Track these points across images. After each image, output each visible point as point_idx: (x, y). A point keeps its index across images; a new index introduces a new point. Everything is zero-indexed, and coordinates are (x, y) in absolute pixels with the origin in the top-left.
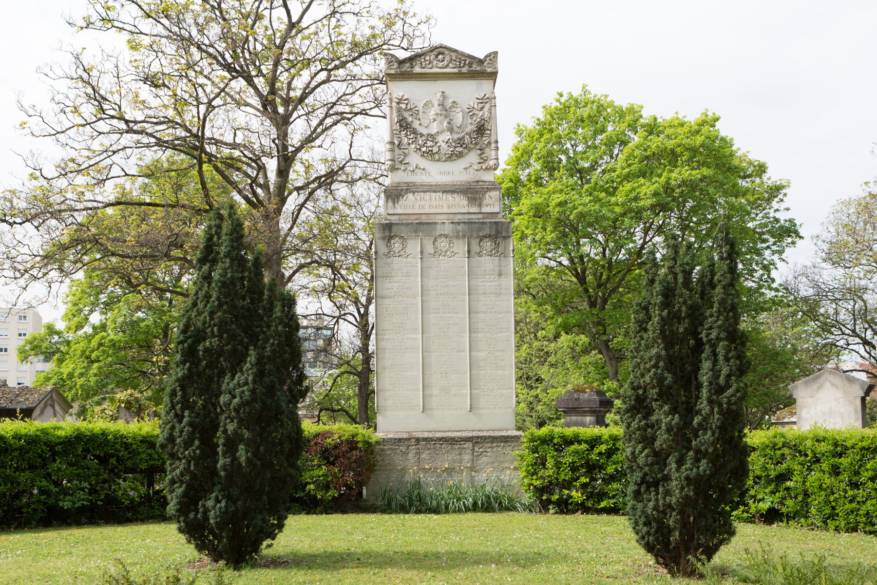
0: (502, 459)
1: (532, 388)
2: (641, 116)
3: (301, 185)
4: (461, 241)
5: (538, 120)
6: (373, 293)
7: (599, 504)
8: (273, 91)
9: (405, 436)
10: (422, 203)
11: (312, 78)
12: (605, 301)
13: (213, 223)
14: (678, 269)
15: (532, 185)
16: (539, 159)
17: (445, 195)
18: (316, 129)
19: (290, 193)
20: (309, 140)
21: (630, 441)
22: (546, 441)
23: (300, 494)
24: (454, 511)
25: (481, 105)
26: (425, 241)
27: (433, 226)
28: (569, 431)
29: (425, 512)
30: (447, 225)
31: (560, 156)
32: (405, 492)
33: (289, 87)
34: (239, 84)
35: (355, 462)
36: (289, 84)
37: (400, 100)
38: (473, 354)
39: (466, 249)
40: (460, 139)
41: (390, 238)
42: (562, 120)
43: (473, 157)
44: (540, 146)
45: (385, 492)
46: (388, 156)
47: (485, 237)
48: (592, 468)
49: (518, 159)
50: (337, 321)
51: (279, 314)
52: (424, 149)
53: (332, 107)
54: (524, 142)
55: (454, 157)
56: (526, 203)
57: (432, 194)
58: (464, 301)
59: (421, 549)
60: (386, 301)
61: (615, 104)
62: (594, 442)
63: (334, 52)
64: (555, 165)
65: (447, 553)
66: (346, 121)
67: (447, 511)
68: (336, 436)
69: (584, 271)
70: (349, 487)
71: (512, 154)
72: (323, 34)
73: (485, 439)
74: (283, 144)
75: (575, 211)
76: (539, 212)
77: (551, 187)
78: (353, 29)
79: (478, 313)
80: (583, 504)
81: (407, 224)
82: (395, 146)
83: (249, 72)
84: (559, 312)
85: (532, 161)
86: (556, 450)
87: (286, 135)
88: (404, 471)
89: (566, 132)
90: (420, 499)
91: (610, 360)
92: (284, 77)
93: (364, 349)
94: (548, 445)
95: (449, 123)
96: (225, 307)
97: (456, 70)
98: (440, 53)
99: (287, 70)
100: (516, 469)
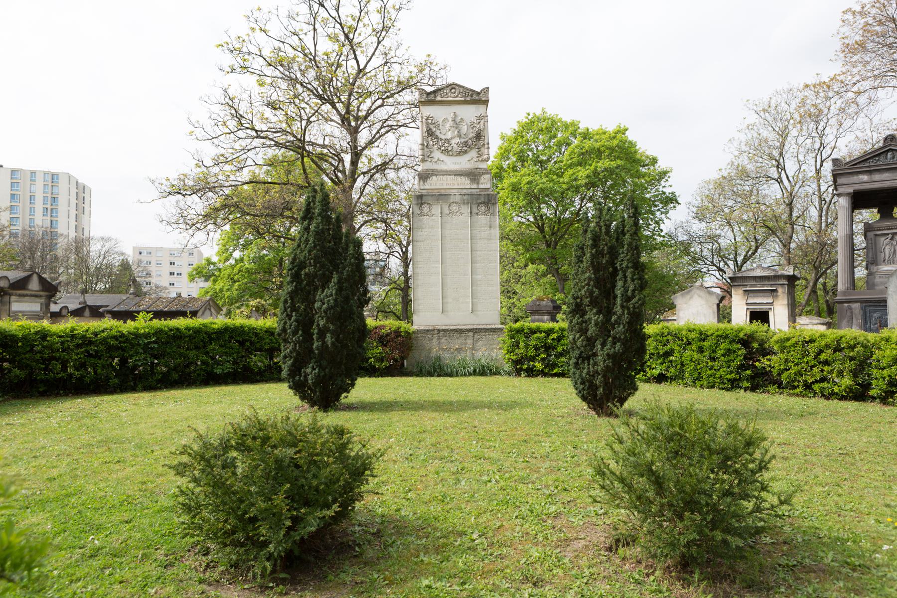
1: (510, 298)
4: (466, 206)
6: (411, 239)
8: (348, 112)
12: (556, 244)
14: (602, 224)
15: (510, 171)
19: (359, 176)
20: (371, 143)
22: (519, 331)
23: (365, 365)
24: (462, 375)
28: (534, 325)
34: (327, 107)
36: (358, 107)
41: (422, 204)
43: (473, 153)
46: (420, 152)
48: (548, 348)
49: (502, 155)
56: (506, 182)
59: (441, 399)
60: (419, 244)
62: (549, 332)
63: (386, 87)
65: (457, 401)
67: (457, 375)
69: (543, 225)
70: (396, 360)
72: (380, 76)
76: (515, 188)
80: (542, 371)
82: (425, 146)
84: (527, 250)
87: (356, 139)
88: (430, 350)
92: (355, 103)
93: (405, 273)
100: (500, 349)
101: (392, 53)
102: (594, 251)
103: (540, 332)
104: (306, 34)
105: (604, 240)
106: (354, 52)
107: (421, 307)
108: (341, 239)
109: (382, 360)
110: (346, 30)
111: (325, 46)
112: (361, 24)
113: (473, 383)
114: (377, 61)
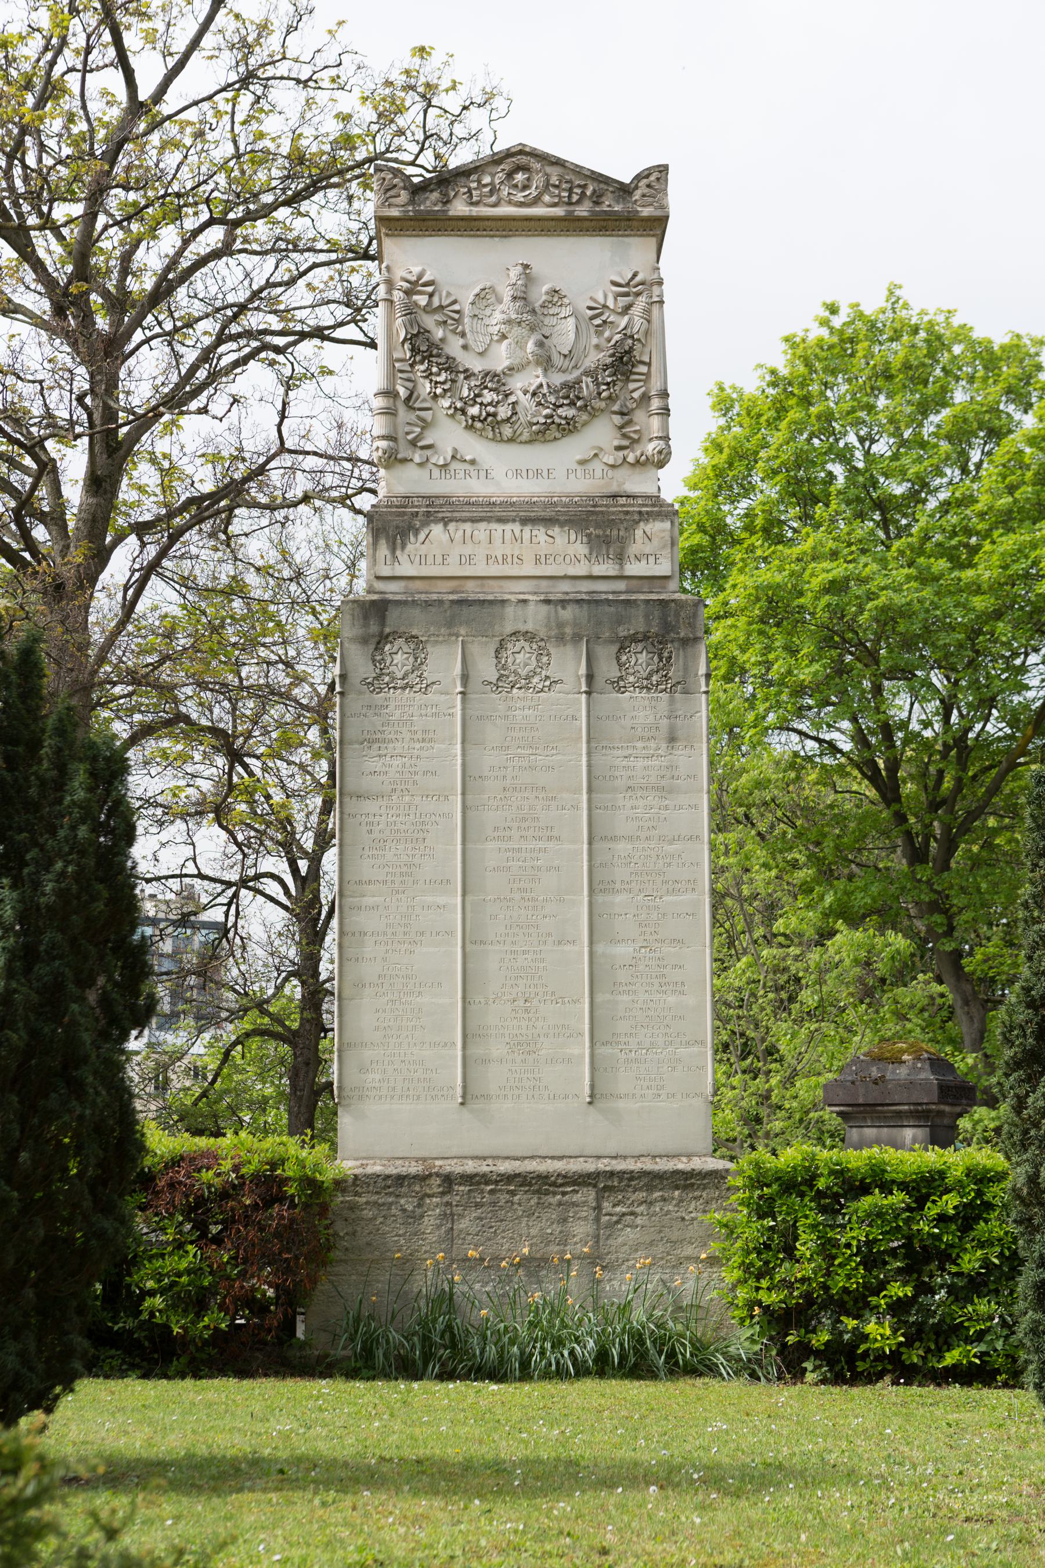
0: (675, 1235)
1: (755, 1074)
3: (147, 517)
4: (569, 650)
5: (773, 372)
6: (333, 822)
7: (941, 1358)
8: (83, 271)
9: (414, 1169)
10: (468, 550)
11: (186, 243)
12: (950, 846)
15: (757, 540)
16: (775, 472)
17: (527, 529)
18: (194, 368)
19: (119, 539)
20: (176, 400)
21: (1025, 1148)
22: (796, 1183)
23: (124, 1323)
24: (546, 1375)
25: (623, 301)
26: (474, 649)
27: (497, 609)
28: (856, 1159)
29: (465, 1377)
30: (531, 607)
31: (830, 467)
32: (411, 1322)
33: (125, 270)
35: (277, 1235)
36: (127, 258)
37: (415, 283)
38: (600, 948)
39: (583, 670)
40: (568, 386)
41: (383, 639)
42: (834, 372)
43: (602, 433)
44: (776, 438)
45: (357, 1320)
46: (378, 426)
47: (634, 639)
48: (921, 1259)
49: (719, 473)
50: (236, 895)
51: (81, 794)
52: (474, 411)
53: (235, 316)
54: (736, 430)
55: (554, 432)
56: (741, 585)
57: (494, 526)
58: (576, 807)
59: (454, 1453)
60: (369, 806)
61: (976, 335)
62: (925, 1187)
63: (244, 179)
64: (817, 490)
65: (525, 1462)
66: (272, 355)
67: (525, 1374)
68: (227, 1165)
69: (893, 766)
70: (259, 1307)
71: (705, 460)
72: (220, 133)
73: (629, 1178)
74: (106, 407)
75: (870, 605)
76: (776, 610)
77: (807, 546)
78: (294, 122)
79: (614, 839)
80: (895, 1356)
81: (428, 604)
82: (396, 400)
83: (20, 215)
84: (827, 874)
85: (756, 479)
86: (823, 1210)
88: (408, 1265)
89: (846, 406)
90: (454, 1340)
91: (966, 1003)
92: (112, 241)
93: (307, 969)
94: (802, 1195)
95: (540, 344)
97: (559, 211)
98: (519, 168)
99: (117, 223)
100: (713, 1261)
101: (273, 43)
103: (886, 1188)
107: (373, 1078)
108: (35, 745)
109: (199, 1303)
113: (596, 1401)
114: (205, 74)
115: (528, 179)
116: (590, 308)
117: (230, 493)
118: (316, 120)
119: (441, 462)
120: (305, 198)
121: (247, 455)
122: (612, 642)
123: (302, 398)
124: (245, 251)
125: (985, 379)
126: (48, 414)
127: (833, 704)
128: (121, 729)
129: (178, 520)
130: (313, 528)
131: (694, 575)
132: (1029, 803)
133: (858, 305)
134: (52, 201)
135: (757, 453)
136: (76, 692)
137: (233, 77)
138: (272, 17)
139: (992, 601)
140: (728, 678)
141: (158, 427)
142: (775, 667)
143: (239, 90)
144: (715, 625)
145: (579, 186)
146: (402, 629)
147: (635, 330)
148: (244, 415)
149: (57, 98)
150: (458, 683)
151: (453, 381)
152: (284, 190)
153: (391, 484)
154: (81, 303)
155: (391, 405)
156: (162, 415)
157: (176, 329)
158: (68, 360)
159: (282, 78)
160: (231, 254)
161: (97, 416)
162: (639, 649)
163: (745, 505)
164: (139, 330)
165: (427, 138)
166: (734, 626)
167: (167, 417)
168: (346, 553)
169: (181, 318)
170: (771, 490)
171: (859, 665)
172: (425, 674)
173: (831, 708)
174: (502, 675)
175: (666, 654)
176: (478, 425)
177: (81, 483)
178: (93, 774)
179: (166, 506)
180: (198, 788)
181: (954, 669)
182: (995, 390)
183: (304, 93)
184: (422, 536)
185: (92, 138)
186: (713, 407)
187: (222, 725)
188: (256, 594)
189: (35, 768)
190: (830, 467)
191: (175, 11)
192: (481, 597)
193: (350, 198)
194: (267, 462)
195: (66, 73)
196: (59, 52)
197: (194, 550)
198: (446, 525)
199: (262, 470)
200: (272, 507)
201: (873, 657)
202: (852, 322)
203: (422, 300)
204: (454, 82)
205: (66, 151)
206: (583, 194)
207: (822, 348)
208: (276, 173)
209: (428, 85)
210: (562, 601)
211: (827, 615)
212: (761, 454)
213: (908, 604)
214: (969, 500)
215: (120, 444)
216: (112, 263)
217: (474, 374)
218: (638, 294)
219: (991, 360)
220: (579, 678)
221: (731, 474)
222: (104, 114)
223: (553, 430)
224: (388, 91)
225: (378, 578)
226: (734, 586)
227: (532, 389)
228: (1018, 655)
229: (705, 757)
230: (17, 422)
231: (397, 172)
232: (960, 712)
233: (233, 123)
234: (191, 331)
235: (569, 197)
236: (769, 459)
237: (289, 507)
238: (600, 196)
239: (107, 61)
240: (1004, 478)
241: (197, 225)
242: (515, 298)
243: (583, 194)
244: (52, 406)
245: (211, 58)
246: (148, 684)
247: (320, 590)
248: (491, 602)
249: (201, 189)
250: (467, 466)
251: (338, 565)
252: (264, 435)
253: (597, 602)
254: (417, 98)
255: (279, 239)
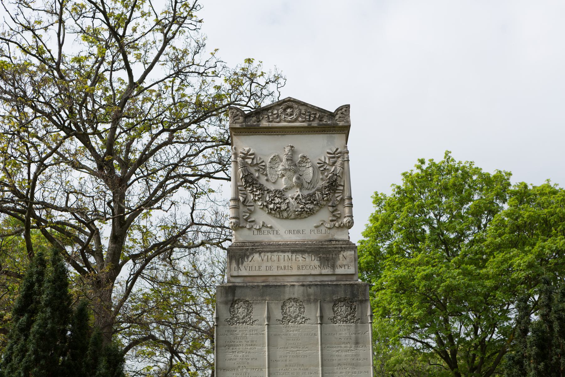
2: (509, 184)
3: (137, 252)
5: (399, 188)
10: (269, 264)
13: (35, 270)
14: (553, 317)
18: (156, 191)
19: (125, 262)
20: (149, 203)
25: (332, 160)
26: (273, 306)
30: (296, 288)
31: (423, 227)
33: (128, 151)
34: (75, 144)
36: (129, 146)
39: (318, 314)
40: (310, 195)
41: (234, 302)
42: (424, 188)
43: (324, 215)
46: (230, 212)
47: (340, 301)
49: (377, 229)
52: (271, 206)
53: (173, 169)
55: (304, 214)
56: (389, 275)
57: (280, 254)
58: (317, 373)
61: (482, 172)
63: (177, 113)
64: (418, 236)
66: (188, 184)
69: (454, 353)
72: (167, 95)
74: (120, 207)
75: (442, 285)
76: (403, 287)
78: (197, 89)
81: (253, 287)
82: (239, 203)
83: (85, 129)
85: (392, 232)
87: (123, 196)
89: (430, 201)
92: (122, 139)
95: (298, 178)
96: (42, 362)
97: (305, 124)
98: (288, 107)
99: (125, 131)
101: (189, 58)
102: (541, 366)
104: (46, 28)
105: (558, 346)
106: (125, 59)
110: (112, 21)
111: (75, 47)
112: (137, 13)
114: (161, 71)
115: (292, 111)
116: (319, 163)
117: (171, 242)
118: (206, 89)
119: (258, 228)
120: (202, 120)
121: (178, 226)
122: (331, 302)
123: (201, 202)
124: (177, 142)
125: (487, 190)
126: (96, 210)
127: (427, 327)
128: (125, 342)
129: (150, 253)
130: (207, 256)
131: (367, 273)
132: (506, 368)
133: (433, 160)
134: (97, 123)
135: (392, 221)
136: (106, 326)
137: (172, 72)
138: (188, 48)
139: (494, 282)
140: (383, 316)
141: (141, 215)
142: (403, 311)
143: (175, 77)
144: (377, 293)
145: (313, 114)
146: (242, 298)
147: (338, 172)
148: (177, 209)
149: (101, 82)
150: (266, 320)
151: (262, 194)
152: (193, 117)
153: (235, 238)
154: (109, 164)
155: (237, 204)
156: (143, 210)
157: (148, 175)
158: (103, 187)
159: (192, 72)
160: (172, 143)
161: (115, 211)
162: (342, 305)
163: (388, 243)
164: (134, 175)
165: (251, 95)
166: (385, 294)
167: (145, 211)
168: (221, 266)
169: (151, 170)
170: (398, 237)
171: (439, 310)
172: (252, 317)
173: (427, 328)
174: (284, 317)
175: (353, 307)
176: (273, 212)
177: (109, 238)
178: (109, 362)
179: (144, 247)
180: (159, 367)
181: (478, 311)
182: (492, 195)
183: (201, 78)
184: (250, 259)
185: (115, 97)
186: (374, 202)
187: (169, 340)
188: (183, 284)
189: (84, 359)
190: (423, 227)
191: (149, 46)
192: (275, 284)
193: (220, 120)
194: (187, 229)
195: (104, 71)
196: (101, 63)
197: (157, 266)
198: (260, 254)
199: (184, 232)
200: (189, 247)
201: (444, 306)
202: (430, 167)
203: (249, 161)
204: (262, 72)
205: (103, 103)
206: (315, 117)
207: (418, 177)
208: (190, 110)
209: (252, 74)
210: (309, 285)
211: (424, 289)
212: (394, 222)
213: (458, 285)
214: (482, 240)
215: (125, 222)
216: (123, 148)
217: (271, 191)
218: (338, 157)
219: (489, 182)
220: (317, 317)
221: (382, 230)
222: (120, 87)
223: (304, 214)
224: (235, 77)
225: (232, 276)
226: (385, 276)
227: (295, 197)
228: (505, 305)
229: (371, 350)
230: (82, 214)
231: (238, 110)
232: (481, 329)
233: (172, 90)
234: (155, 175)
235: (309, 118)
236: (398, 224)
237: (196, 247)
238: (322, 118)
239: (121, 66)
240: (497, 231)
241: (158, 132)
242: (287, 160)
243: (315, 117)
244: (97, 207)
245: (163, 64)
246: (136, 323)
247: (208, 281)
248: (279, 286)
249: (160, 117)
250: (269, 229)
251: (217, 271)
252: (185, 217)
253: (324, 285)
254: (248, 79)
255: (191, 137)
